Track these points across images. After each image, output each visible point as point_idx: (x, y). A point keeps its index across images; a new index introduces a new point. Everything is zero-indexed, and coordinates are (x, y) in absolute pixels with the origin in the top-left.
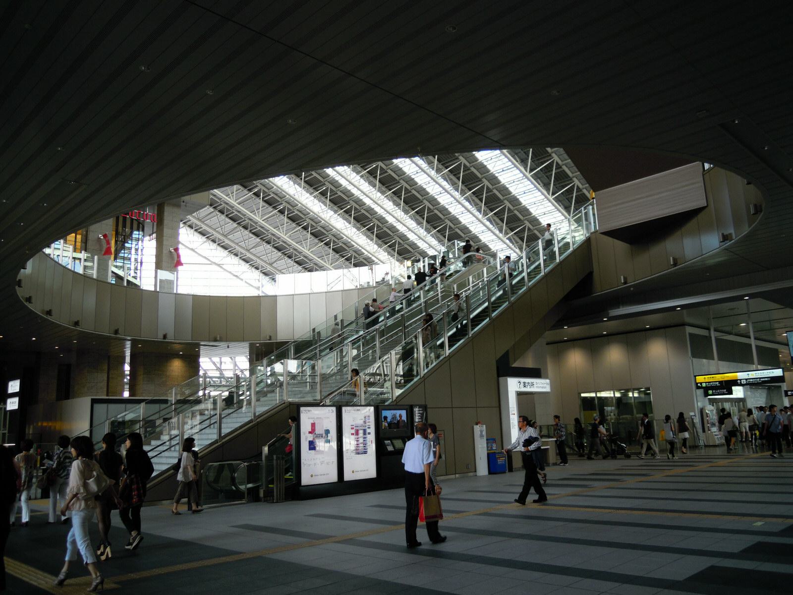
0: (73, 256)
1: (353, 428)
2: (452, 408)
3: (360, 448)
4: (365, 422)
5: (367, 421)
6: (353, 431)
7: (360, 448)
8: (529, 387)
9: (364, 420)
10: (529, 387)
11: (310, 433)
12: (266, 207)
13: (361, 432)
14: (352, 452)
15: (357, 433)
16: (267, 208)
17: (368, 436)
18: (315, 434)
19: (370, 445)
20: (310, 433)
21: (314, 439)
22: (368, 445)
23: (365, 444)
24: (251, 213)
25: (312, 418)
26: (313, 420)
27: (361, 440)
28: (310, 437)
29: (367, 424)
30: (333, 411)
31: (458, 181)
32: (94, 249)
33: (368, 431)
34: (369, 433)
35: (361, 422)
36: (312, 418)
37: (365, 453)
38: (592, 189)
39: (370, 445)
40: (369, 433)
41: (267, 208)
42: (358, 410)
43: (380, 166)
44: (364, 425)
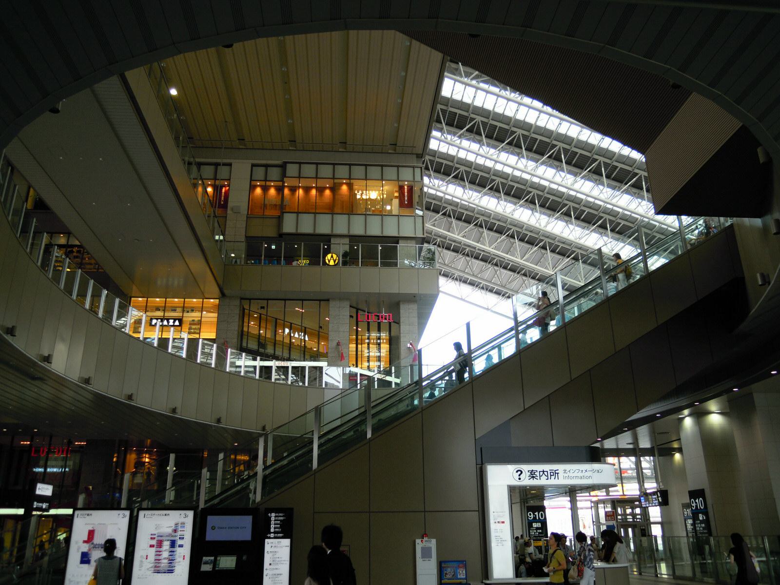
0: (246, 365)
1: (155, 538)
2: (370, 512)
3: (163, 565)
4: (175, 531)
5: (180, 529)
6: (154, 542)
7: (163, 565)
8: (544, 477)
9: (173, 528)
10: (544, 477)
11: (85, 542)
12: (592, 271)
13: (166, 545)
14: (148, 569)
15: (160, 544)
16: (594, 270)
17: (179, 550)
18: (93, 544)
19: (180, 562)
20: (85, 542)
21: (90, 550)
22: (177, 561)
23: (171, 561)
24: (565, 276)
25: (91, 524)
26: (92, 526)
27: (165, 554)
28: (85, 548)
29: (179, 533)
30: (124, 516)
31: (520, 149)
32: (332, 357)
33: (179, 542)
34: (181, 546)
35: (170, 530)
36: (91, 524)
37: (171, 571)
38: (508, 85)
39: (180, 562)
40: (181, 546)
41: (594, 270)
42: (166, 515)
43: (603, 162)
44: (174, 534)
